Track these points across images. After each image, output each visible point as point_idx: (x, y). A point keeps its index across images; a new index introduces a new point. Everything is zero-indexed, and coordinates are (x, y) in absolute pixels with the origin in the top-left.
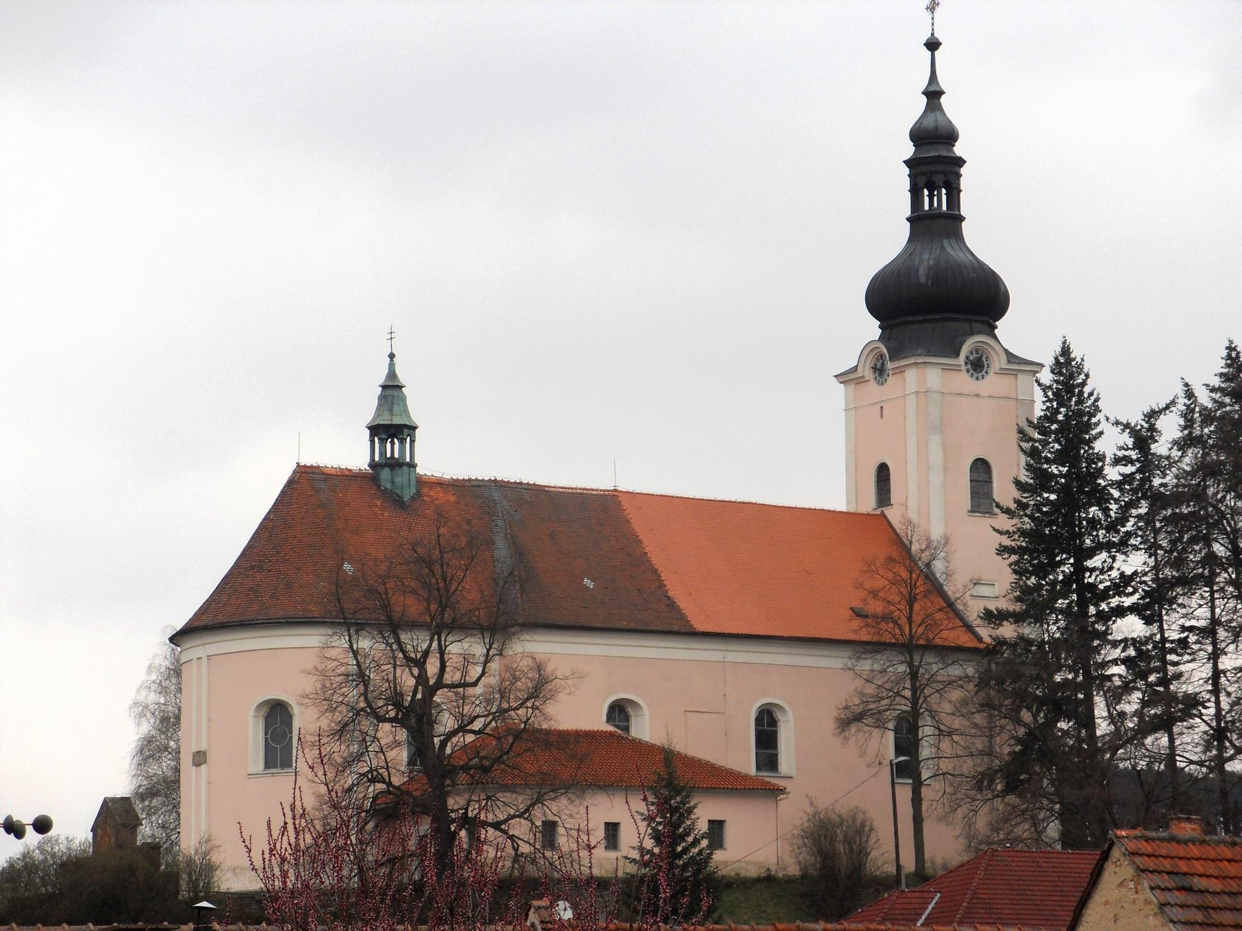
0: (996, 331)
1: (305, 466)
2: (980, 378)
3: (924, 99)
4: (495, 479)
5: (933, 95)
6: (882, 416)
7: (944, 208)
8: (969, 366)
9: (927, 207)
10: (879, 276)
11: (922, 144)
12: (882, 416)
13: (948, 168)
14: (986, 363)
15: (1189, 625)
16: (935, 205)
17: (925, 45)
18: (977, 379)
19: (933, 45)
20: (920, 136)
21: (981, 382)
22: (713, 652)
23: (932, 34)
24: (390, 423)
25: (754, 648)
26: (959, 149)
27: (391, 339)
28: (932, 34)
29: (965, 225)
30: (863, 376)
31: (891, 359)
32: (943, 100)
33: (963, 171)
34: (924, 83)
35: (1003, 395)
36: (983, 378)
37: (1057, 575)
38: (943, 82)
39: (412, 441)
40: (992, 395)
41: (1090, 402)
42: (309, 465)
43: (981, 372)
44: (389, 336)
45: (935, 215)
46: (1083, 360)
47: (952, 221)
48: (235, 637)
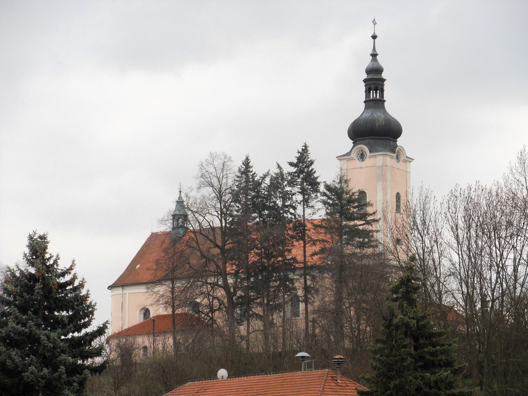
1: (154, 233)
3: (371, 57)
5: (374, 55)
7: (378, 97)
9: (371, 97)
11: (369, 75)
13: (380, 82)
15: (64, 281)
17: (371, 37)
19: (374, 37)
20: (369, 71)
21: (364, 162)
23: (374, 33)
26: (384, 75)
28: (374, 33)
30: (353, 158)
32: (377, 57)
33: (385, 83)
35: (372, 165)
37: (251, 238)
38: (378, 51)
40: (367, 166)
42: (155, 232)
45: (375, 100)
46: (65, 268)
47: (381, 101)
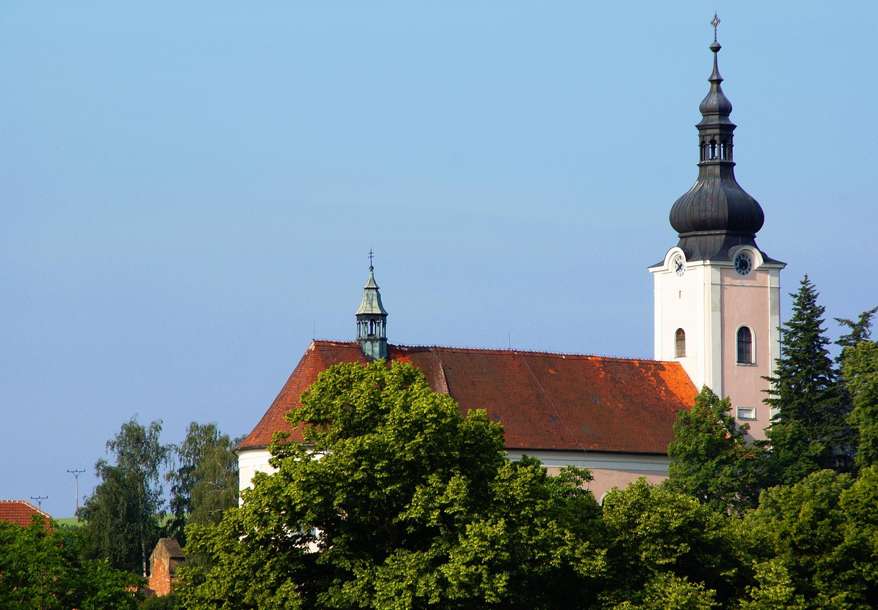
0: (755, 239)
2: (745, 273)
4: (435, 346)
5: (716, 82)
6: (680, 297)
8: (738, 263)
10: (674, 211)
12: (680, 297)
14: (749, 263)
16: (716, 154)
18: (743, 274)
19: (716, 49)
22: (663, 466)
23: (716, 41)
24: (371, 312)
25: (607, 459)
27: (371, 257)
29: (736, 169)
31: (687, 260)
33: (734, 132)
34: (709, 72)
36: (747, 273)
39: (384, 324)
41: (799, 307)
43: (745, 269)
44: (369, 255)
47: (727, 168)
48: (621, 460)
